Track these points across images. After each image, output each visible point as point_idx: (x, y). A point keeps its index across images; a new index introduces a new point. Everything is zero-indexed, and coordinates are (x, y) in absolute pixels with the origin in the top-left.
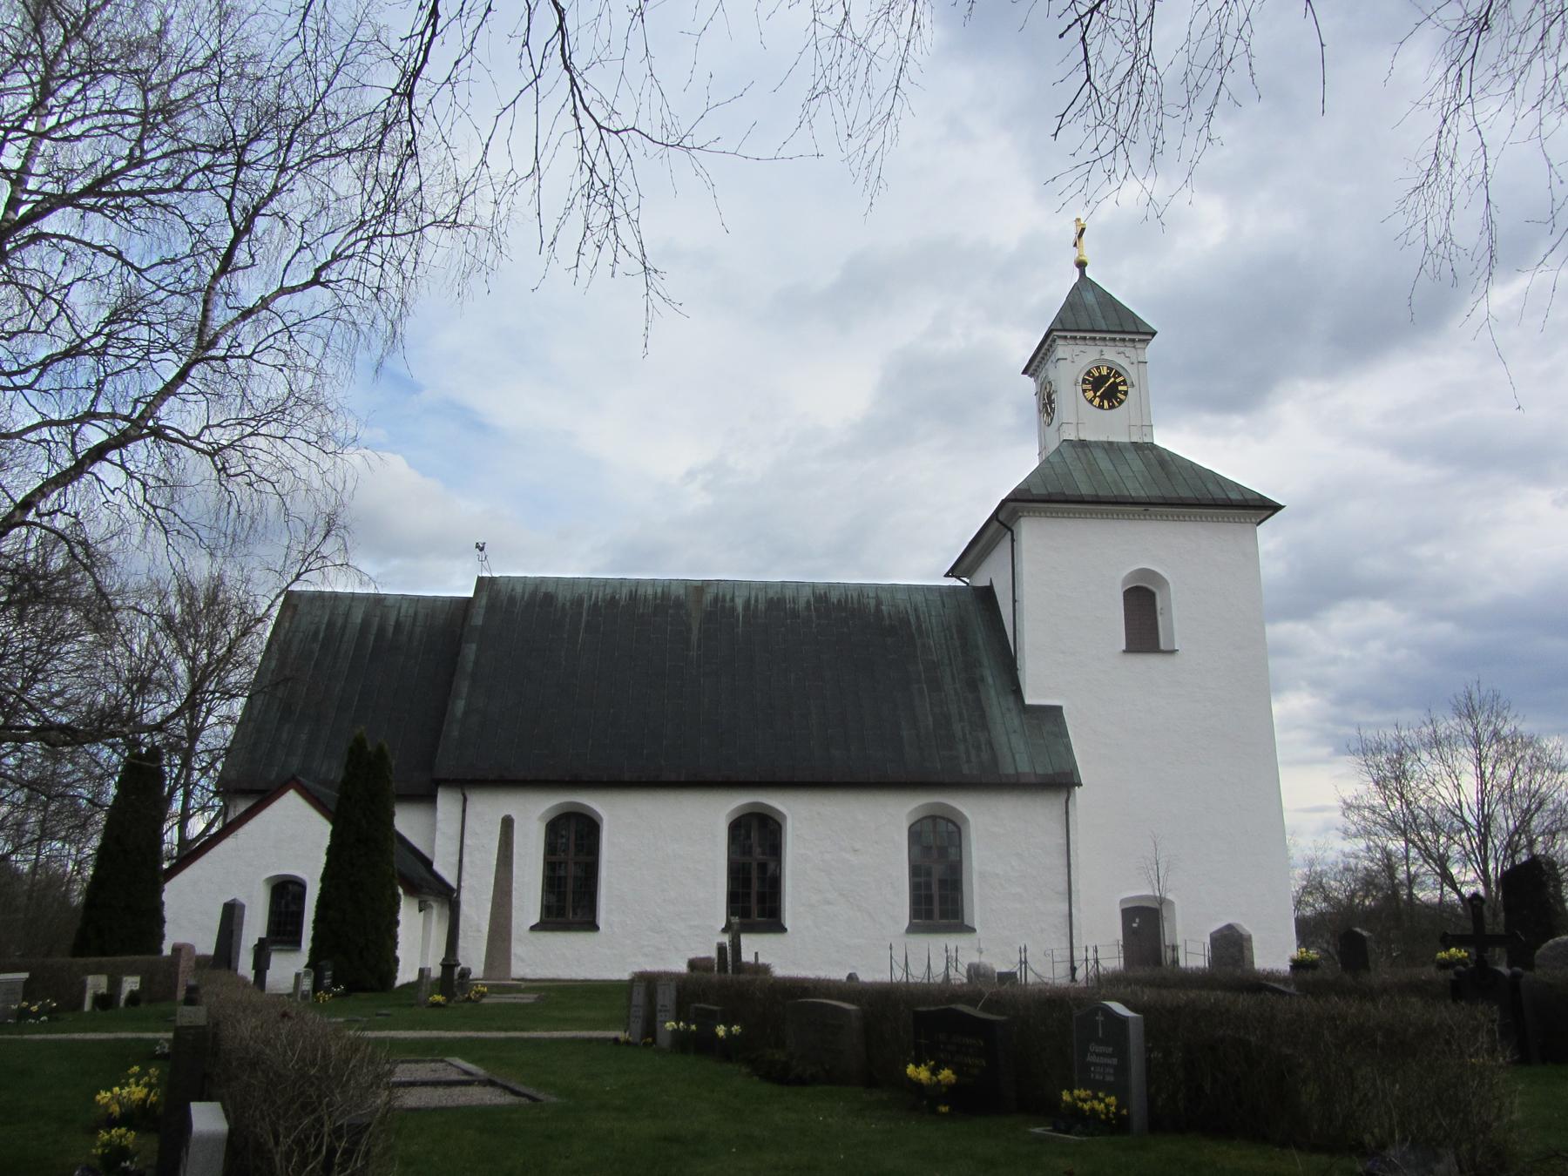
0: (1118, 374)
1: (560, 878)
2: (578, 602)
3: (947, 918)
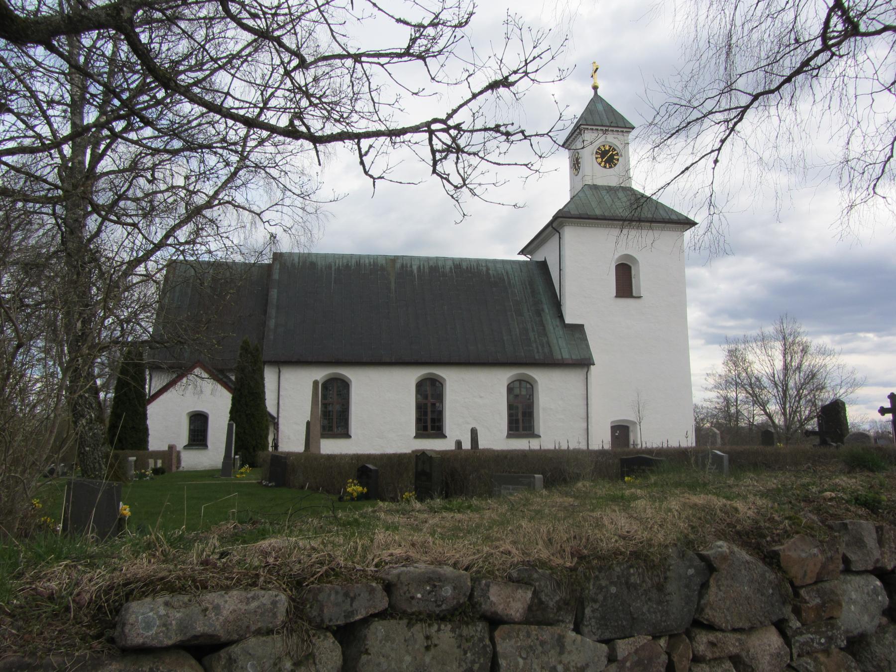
0: (614, 150)
1: (330, 411)
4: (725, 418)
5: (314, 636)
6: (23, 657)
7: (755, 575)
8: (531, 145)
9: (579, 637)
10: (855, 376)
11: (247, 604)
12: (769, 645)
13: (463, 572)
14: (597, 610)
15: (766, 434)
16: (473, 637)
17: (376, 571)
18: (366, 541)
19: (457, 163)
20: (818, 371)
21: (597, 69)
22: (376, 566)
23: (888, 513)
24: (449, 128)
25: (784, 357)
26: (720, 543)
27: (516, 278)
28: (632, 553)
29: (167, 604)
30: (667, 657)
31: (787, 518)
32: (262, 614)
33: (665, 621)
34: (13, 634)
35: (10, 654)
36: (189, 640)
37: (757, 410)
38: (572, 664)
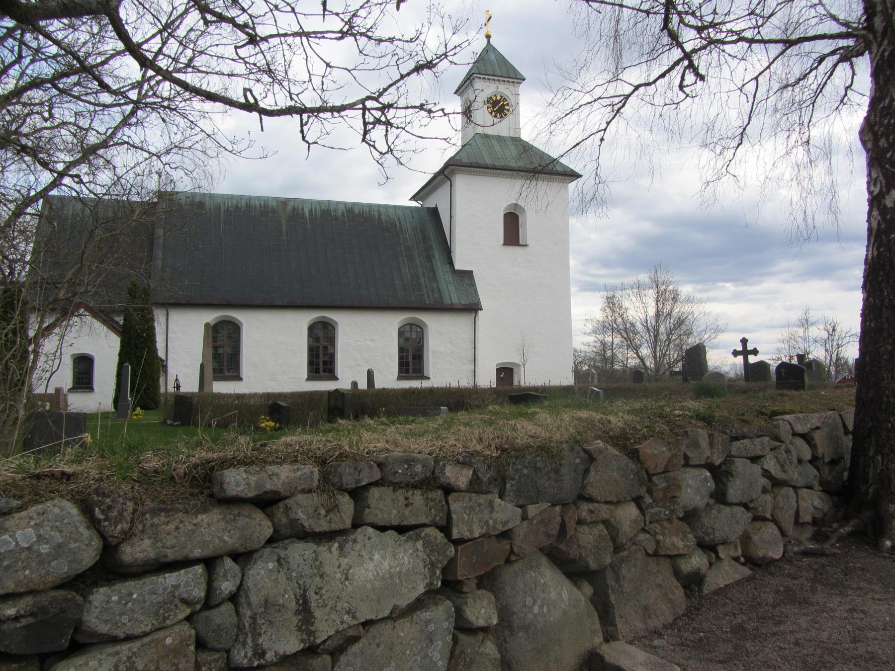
0: (505, 100)
1: (220, 354)
9: (503, 502)
10: (718, 323)
15: (637, 374)
20: (686, 318)
21: (490, 18)
25: (657, 304)
27: (408, 224)
29: (245, 471)
31: (645, 427)
36: (261, 495)
37: (631, 354)
38: (499, 520)
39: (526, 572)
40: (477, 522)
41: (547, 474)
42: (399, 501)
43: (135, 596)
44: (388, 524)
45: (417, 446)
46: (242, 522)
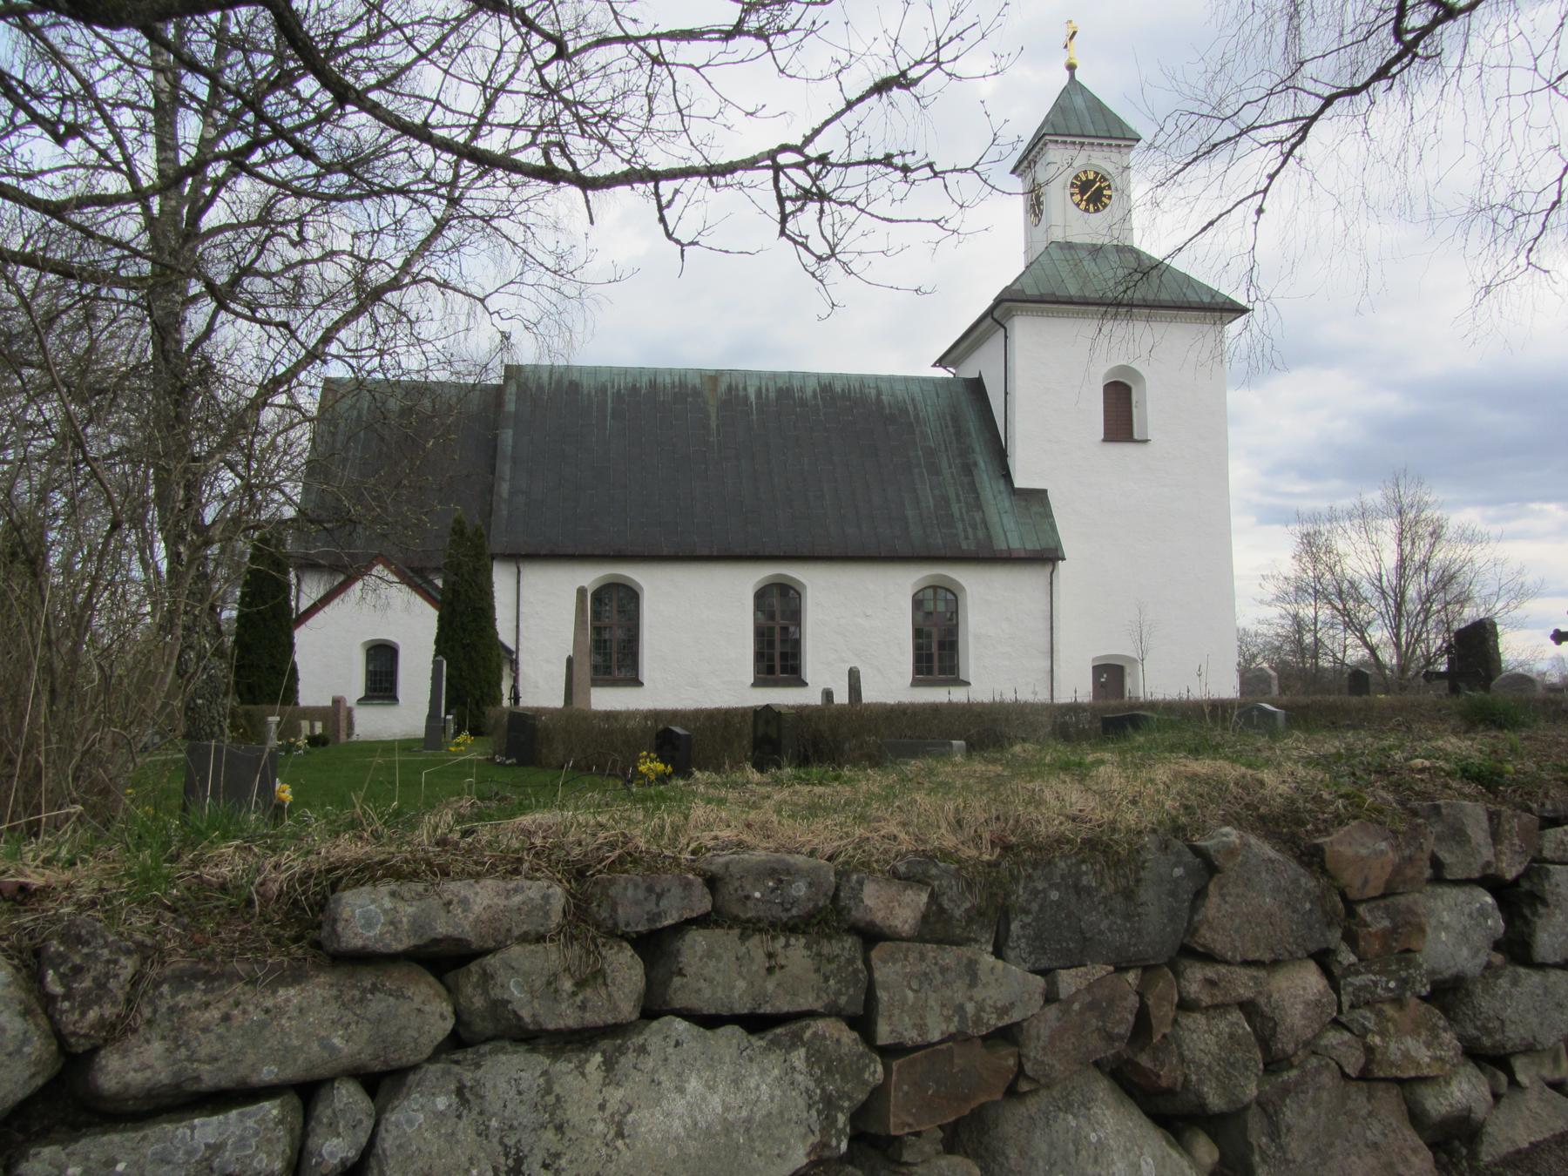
0: (1104, 179)
1: (605, 641)
2: (603, 390)
3: (945, 673)
4: (1294, 652)
5: (604, 945)
6: (198, 963)
7: (1283, 882)
8: (946, 187)
9: (1000, 963)
11: (507, 898)
12: (1304, 989)
13: (823, 861)
14: (1030, 924)
15: (1358, 679)
16: (838, 956)
17: (693, 861)
18: (678, 818)
19: (820, 220)
21: (1074, 33)
22: (693, 853)
23: (1514, 791)
24: (808, 161)
25: (1399, 545)
26: (1227, 829)
27: (929, 409)
28: (1084, 842)
29: (393, 894)
30: (1137, 998)
31: (1341, 796)
32: (529, 913)
33: (1135, 945)
34: (178, 934)
35: (178, 958)
36: (426, 946)
37: (1352, 639)
38: (990, 1002)
39: (1056, 1118)
40: (937, 1008)
41: (1105, 900)
42: (752, 960)
43: (120, 1167)
44: (725, 1012)
45: (810, 837)
46: (378, 1004)
